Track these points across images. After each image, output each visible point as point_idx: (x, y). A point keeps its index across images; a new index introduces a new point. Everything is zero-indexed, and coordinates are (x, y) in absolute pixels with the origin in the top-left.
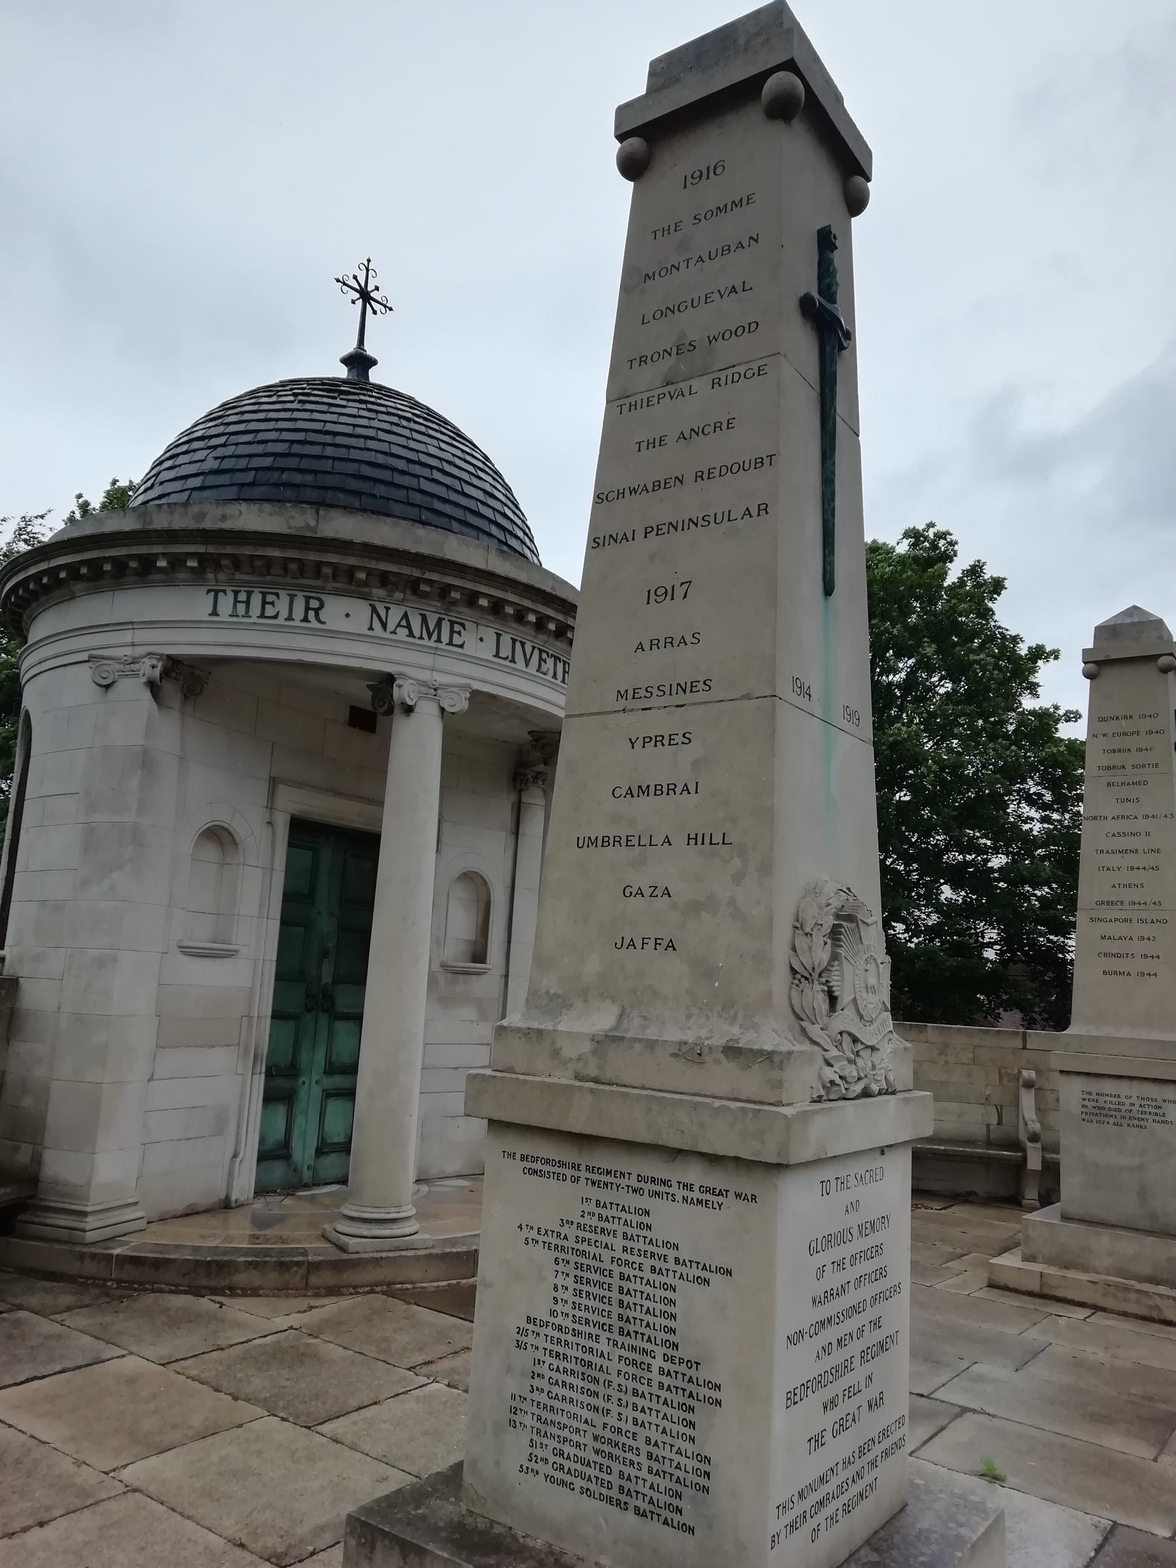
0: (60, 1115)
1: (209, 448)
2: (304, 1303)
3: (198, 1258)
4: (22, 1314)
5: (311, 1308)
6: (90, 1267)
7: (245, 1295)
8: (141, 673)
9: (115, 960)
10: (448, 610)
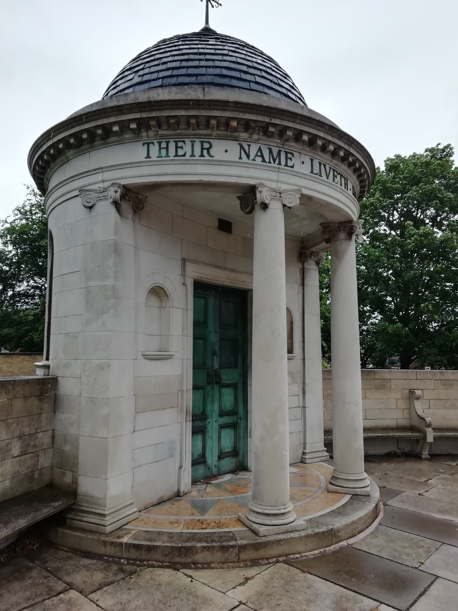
0: (86, 456)
1: (134, 72)
2: (239, 574)
3: (174, 545)
4: (73, 594)
5: (247, 579)
6: (110, 550)
7: (203, 568)
8: (109, 197)
9: (109, 366)
10: (283, 144)
